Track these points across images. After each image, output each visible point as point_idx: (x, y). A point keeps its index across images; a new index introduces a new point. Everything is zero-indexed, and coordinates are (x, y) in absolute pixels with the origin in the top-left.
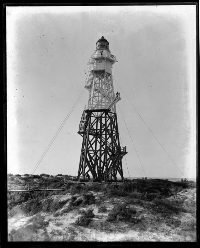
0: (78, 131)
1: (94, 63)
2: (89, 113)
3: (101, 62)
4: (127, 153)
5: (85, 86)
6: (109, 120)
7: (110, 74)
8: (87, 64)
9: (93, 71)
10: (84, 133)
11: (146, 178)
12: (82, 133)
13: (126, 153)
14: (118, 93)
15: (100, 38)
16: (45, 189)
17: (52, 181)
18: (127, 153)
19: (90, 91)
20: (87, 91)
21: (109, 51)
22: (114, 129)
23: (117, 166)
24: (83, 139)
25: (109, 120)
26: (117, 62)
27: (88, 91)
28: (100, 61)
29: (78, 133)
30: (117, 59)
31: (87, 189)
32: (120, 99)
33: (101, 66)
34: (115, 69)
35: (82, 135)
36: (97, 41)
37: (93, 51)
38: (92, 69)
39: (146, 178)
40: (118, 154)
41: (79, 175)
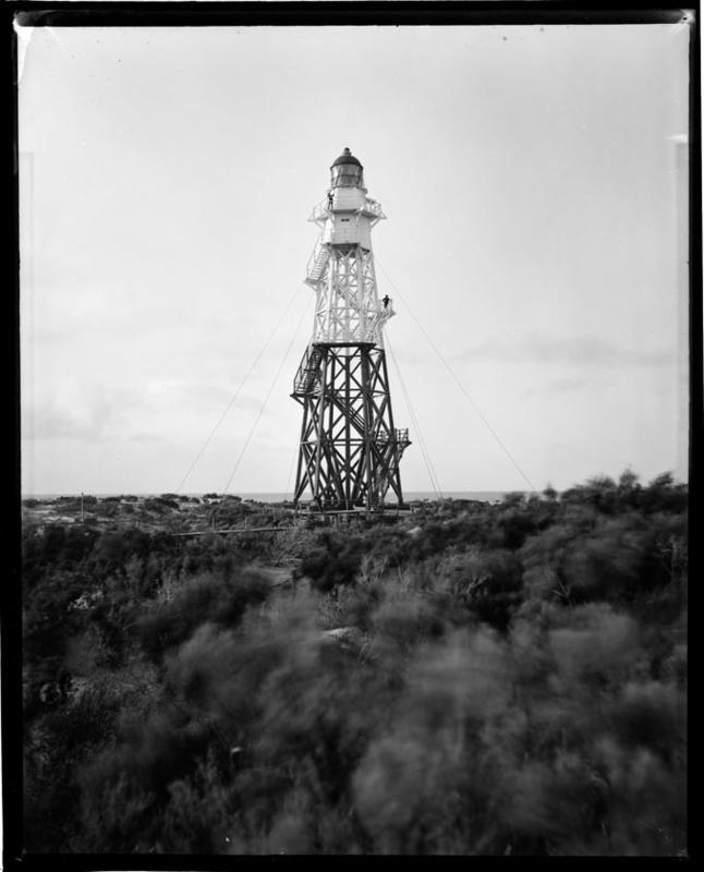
0: (292, 392)
1: (326, 219)
2: (322, 351)
3: (348, 220)
4: (410, 443)
5: (307, 279)
6: (344, 418)
7: (368, 251)
8: (309, 221)
9: (329, 244)
10: (305, 395)
11: (551, 493)
12: (301, 396)
13: (408, 443)
14: (386, 300)
15: (340, 153)
16: (227, 529)
17: (238, 513)
18: (410, 443)
19: (318, 291)
20: (310, 291)
21: (365, 191)
22: (379, 387)
23: (391, 475)
24: (303, 411)
25: (344, 418)
26: (385, 218)
27: (312, 290)
28: (345, 218)
29: (292, 396)
30: (385, 211)
31: (227, 516)
32: (393, 314)
33: (349, 232)
34: (378, 238)
35: (302, 400)
36: (332, 164)
37: (323, 177)
38: (327, 239)
39: (628, 478)
40: (384, 450)
41: (300, 489)
